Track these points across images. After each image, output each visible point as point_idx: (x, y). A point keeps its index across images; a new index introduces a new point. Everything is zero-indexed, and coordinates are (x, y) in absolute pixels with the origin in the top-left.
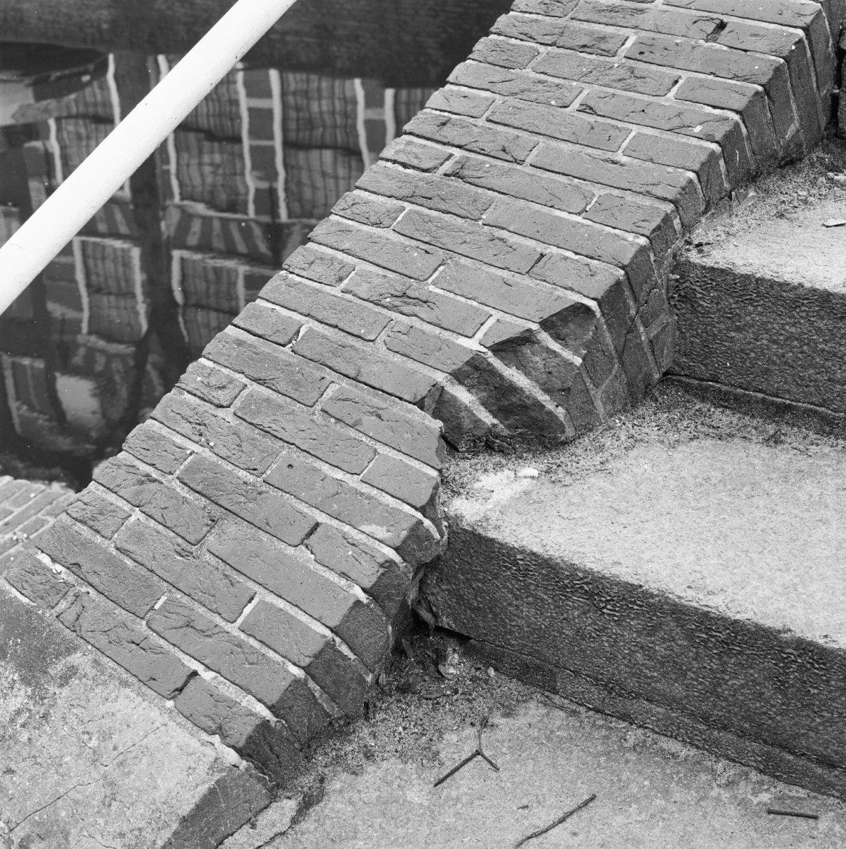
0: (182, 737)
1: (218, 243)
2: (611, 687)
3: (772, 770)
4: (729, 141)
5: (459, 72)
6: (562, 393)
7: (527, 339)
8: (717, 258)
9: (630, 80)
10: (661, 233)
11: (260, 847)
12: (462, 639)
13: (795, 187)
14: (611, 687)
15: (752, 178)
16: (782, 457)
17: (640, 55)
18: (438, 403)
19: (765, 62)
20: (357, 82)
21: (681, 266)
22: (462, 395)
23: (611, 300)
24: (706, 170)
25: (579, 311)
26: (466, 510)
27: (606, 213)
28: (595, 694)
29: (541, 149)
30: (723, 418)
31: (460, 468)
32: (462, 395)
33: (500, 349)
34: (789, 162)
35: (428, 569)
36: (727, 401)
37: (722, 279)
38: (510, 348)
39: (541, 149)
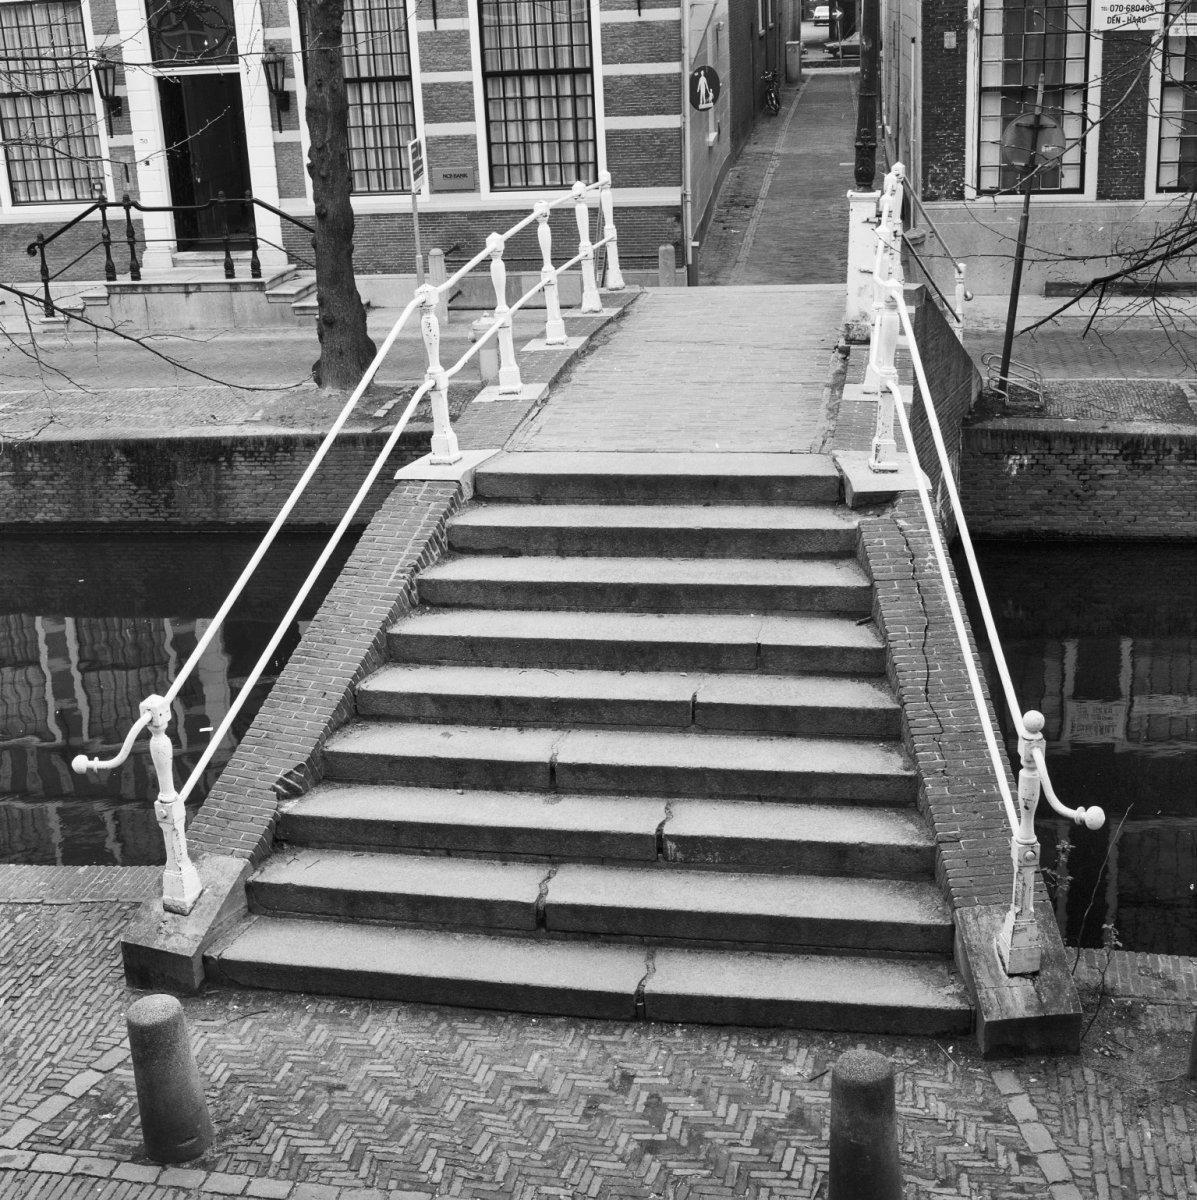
0: (235, 860)
1: (34, 784)
2: (320, 842)
3: (354, 850)
4: (330, 722)
5: (261, 709)
6: (300, 783)
7: (291, 773)
8: (330, 749)
9: (306, 709)
10: (317, 745)
11: (136, 1198)
12: (286, 841)
13: (348, 729)
14: (320, 842)
15: (337, 729)
16: (350, 790)
17: (307, 701)
18: (274, 789)
19: (336, 702)
20: (69, 621)
21: (323, 752)
22: (279, 787)
23: (308, 761)
24: (325, 730)
25: (302, 765)
26: (283, 810)
27: (304, 742)
28: (317, 845)
29: (286, 729)
30: (337, 785)
31: (281, 803)
32: (279, 787)
33: (285, 776)
34: (346, 723)
35: (278, 823)
36: (338, 781)
37: (332, 754)
38: (287, 775)
39: (286, 729)
